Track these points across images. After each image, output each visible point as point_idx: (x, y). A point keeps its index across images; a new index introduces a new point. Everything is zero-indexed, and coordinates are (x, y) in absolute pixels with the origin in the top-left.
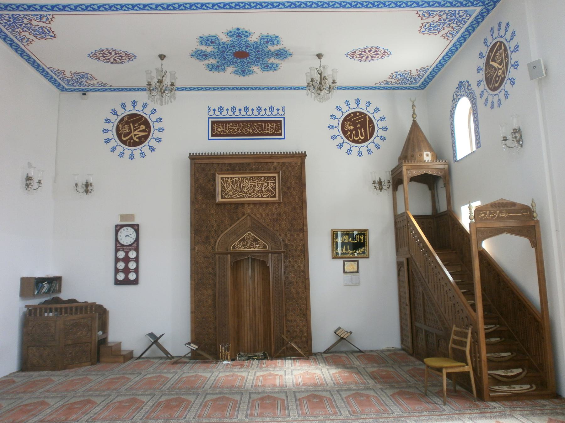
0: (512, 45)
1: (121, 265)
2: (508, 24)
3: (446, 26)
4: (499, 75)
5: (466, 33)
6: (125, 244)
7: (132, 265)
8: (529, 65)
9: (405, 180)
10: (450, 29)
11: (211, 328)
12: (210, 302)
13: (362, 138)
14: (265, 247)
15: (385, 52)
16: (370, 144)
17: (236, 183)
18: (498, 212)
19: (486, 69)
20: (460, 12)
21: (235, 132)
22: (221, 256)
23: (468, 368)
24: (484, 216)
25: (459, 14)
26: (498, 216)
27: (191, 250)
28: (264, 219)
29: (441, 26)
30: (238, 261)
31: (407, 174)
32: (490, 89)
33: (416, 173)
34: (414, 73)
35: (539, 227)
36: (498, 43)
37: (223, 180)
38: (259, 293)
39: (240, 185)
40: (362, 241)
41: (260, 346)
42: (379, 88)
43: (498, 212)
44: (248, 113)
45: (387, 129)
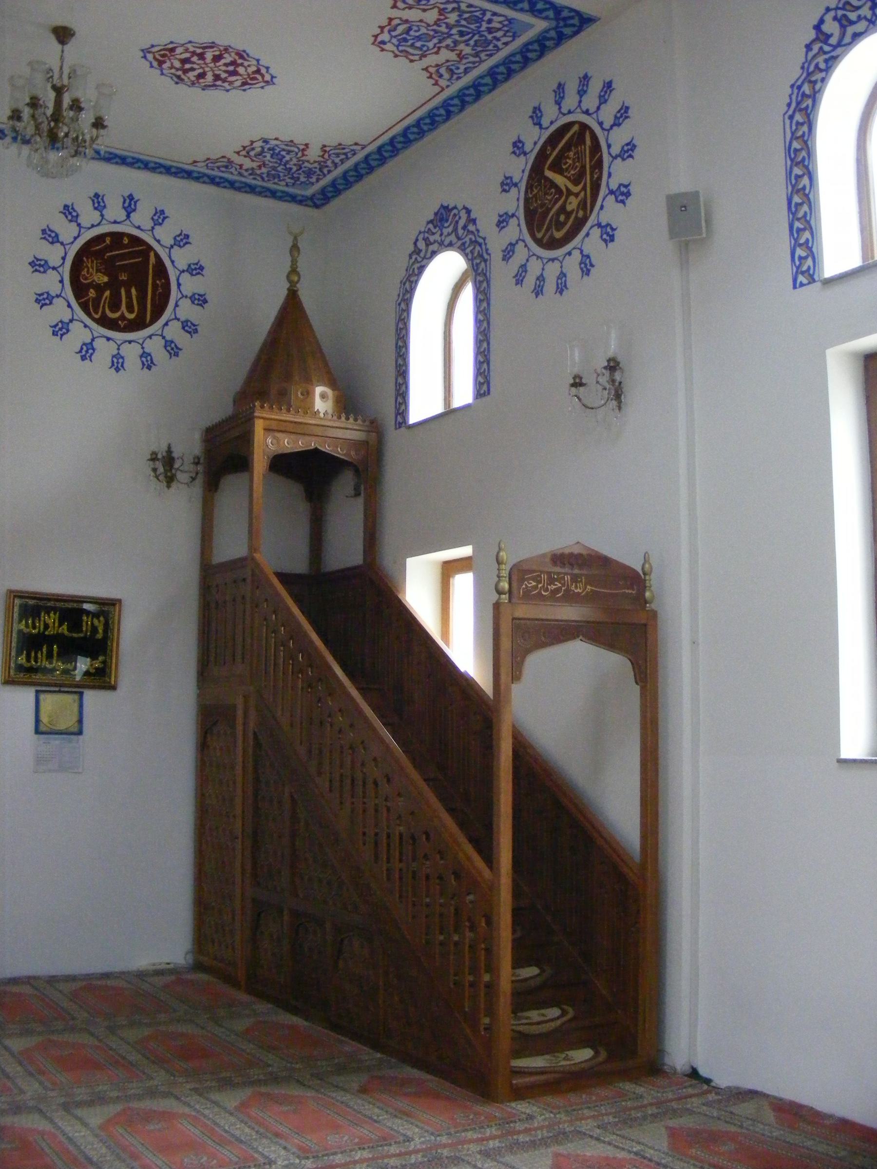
0: (618, 138)
2: (608, 86)
3: (447, 47)
4: (569, 208)
5: (488, 80)
8: (671, 200)
9: (260, 464)
10: (453, 56)
13: (131, 316)
15: (258, 71)
16: (150, 339)
19: (529, 187)
20: (495, 18)
24: (536, 587)
25: (490, 21)
26: (568, 591)
29: (435, 41)
31: (266, 443)
32: (539, 242)
33: (288, 444)
34: (313, 154)
35: (655, 626)
36: (576, 128)
40: (100, 636)
42: (199, 178)
43: (568, 578)
45: (205, 301)
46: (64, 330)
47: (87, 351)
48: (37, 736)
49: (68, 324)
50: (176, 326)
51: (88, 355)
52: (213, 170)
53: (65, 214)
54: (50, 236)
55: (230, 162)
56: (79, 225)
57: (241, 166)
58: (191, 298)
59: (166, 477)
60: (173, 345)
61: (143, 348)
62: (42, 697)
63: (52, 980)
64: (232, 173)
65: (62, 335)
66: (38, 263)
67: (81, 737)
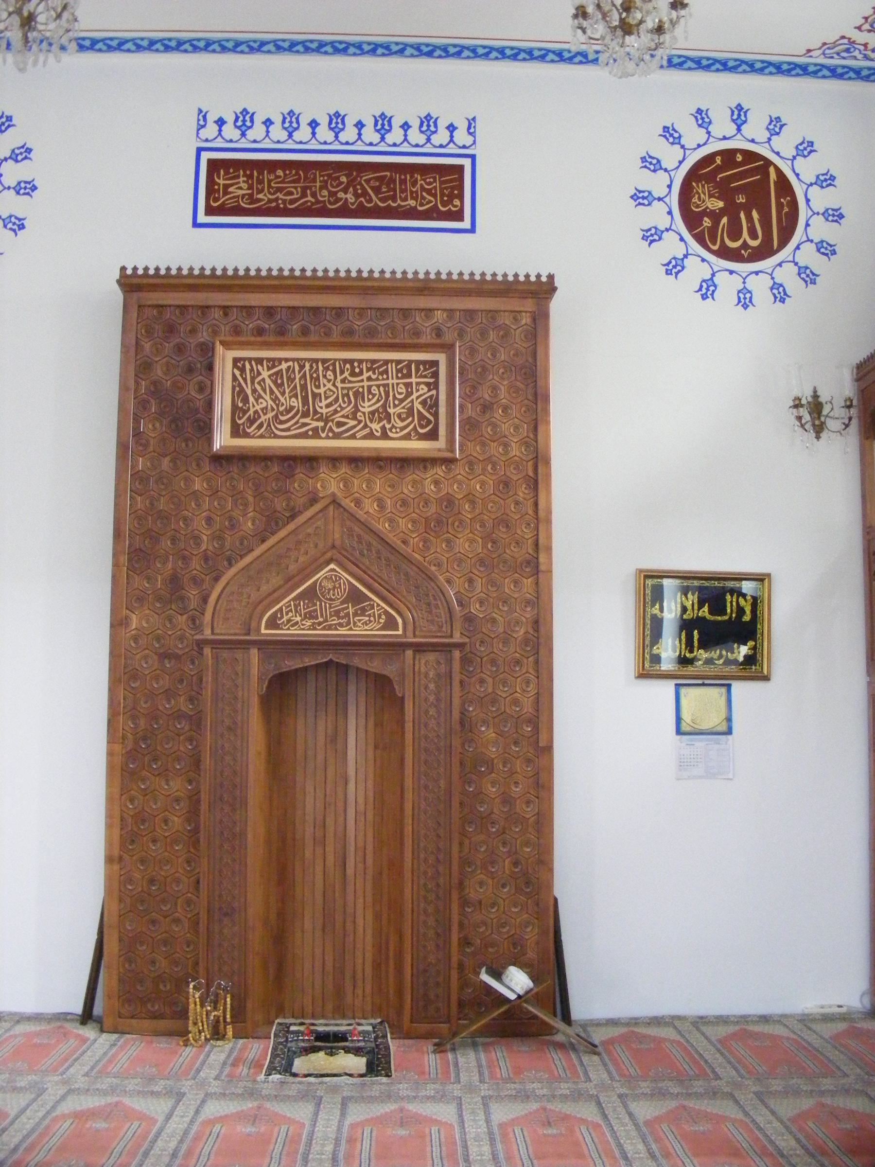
11: (177, 921)
12: (176, 821)
13: (754, 243)
14: (390, 624)
16: (780, 267)
17: (291, 380)
21: (292, 202)
22: (225, 654)
27: (112, 626)
28: (391, 521)
37: (242, 370)
38: (361, 800)
39: (304, 387)
40: (747, 618)
41: (359, 991)
44: (343, 137)
45: (841, 216)
46: (679, 268)
47: (707, 289)
48: (679, 737)
49: (682, 260)
50: (808, 249)
51: (709, 293)
52: (832, 57)
53: (665, 136)
54: (651, 163)
55: (852, 42)
56: (683, 147)
57: (865, 45)
58: (823, 214)
59: (814, 425)
60: (808, 272)
61: (773, 278)
62: (683, 691)
63: (700, 1022)
64: (855, 58)
65: (677, 274)
66: (641, 195)
67: (729, 737)
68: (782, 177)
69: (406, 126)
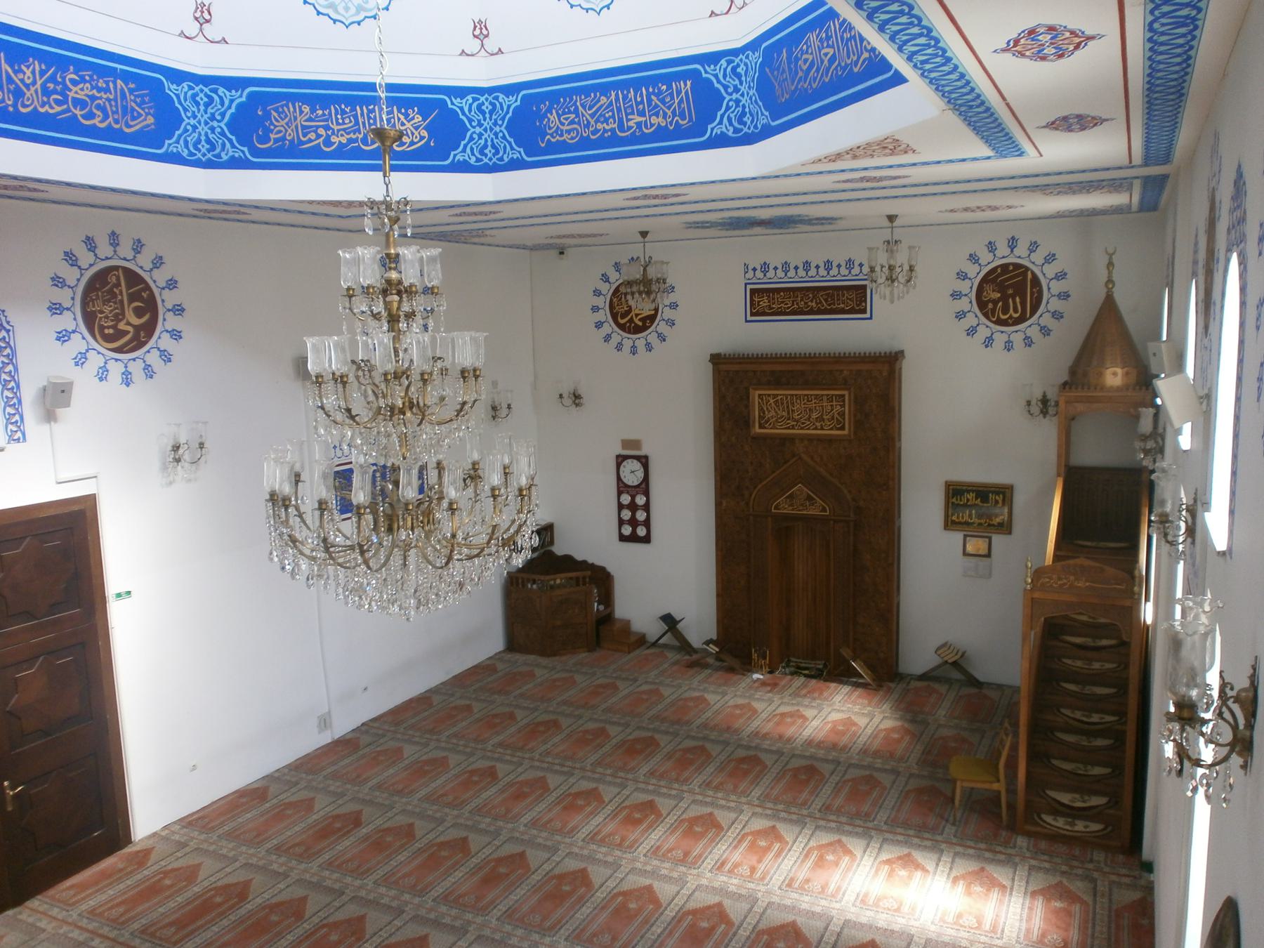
1: (626, 514)
6: (630, 483)
7: (641, 516)
13: (1016, 315)
14: (824, 510)
16: (1030, 328)
18: (1072, 578)
23: (1000, 786)
30: (785, 528)
68: (1035, 277)
69: (839, 266)
